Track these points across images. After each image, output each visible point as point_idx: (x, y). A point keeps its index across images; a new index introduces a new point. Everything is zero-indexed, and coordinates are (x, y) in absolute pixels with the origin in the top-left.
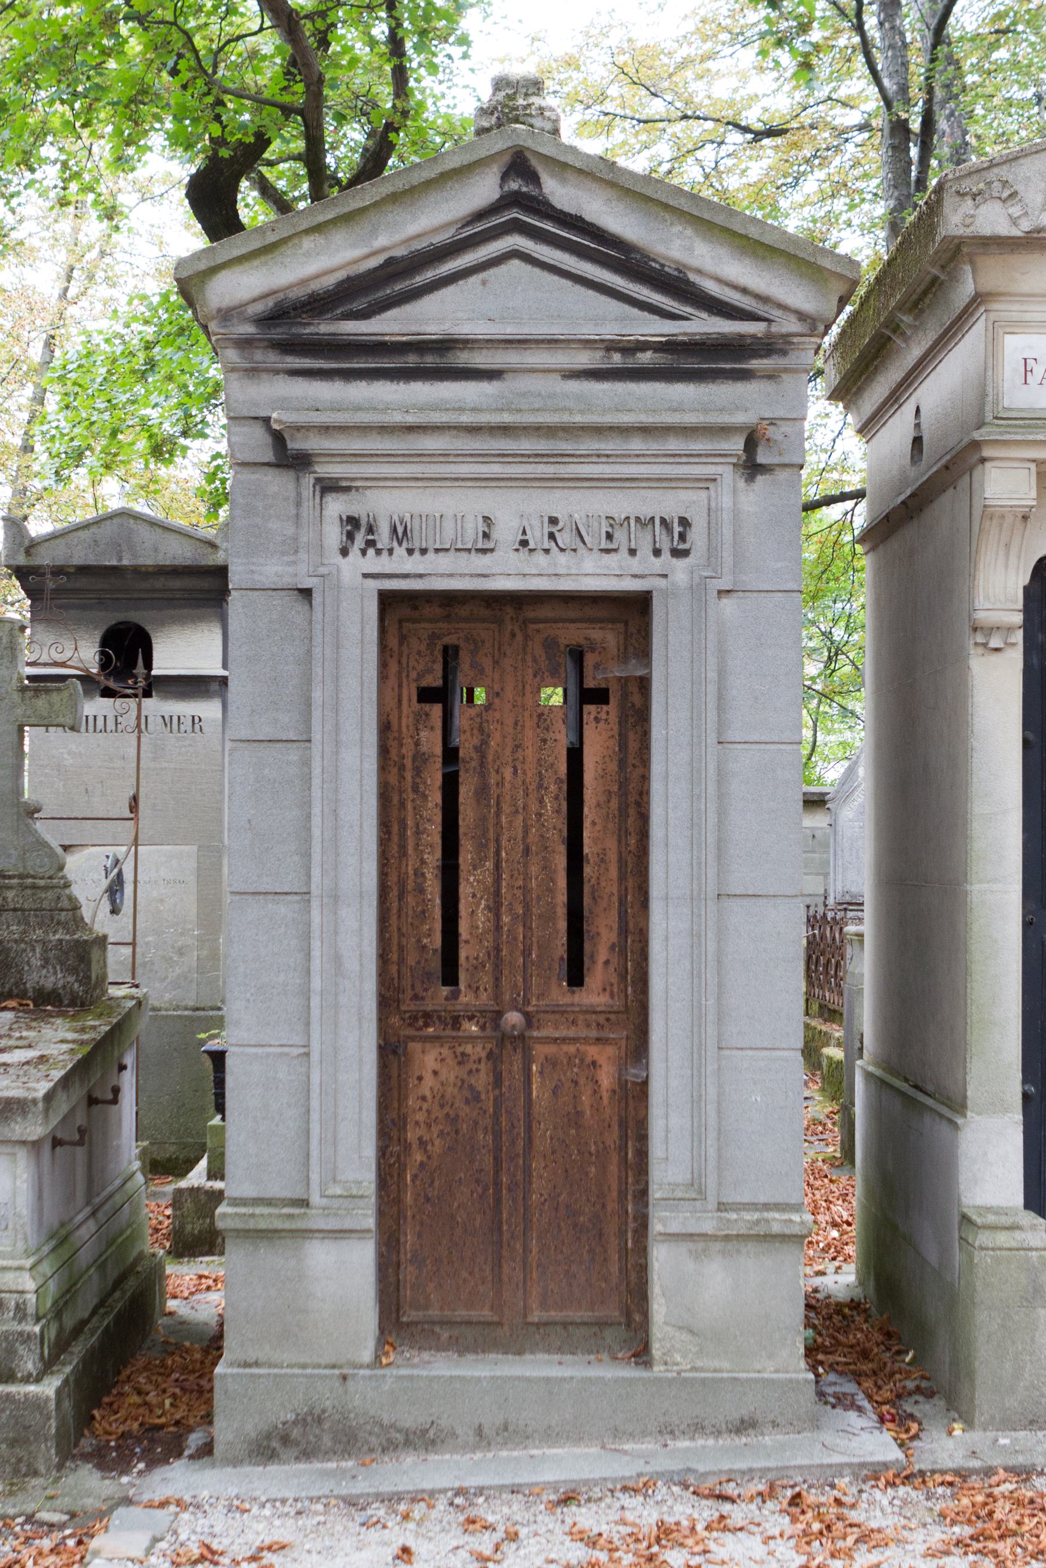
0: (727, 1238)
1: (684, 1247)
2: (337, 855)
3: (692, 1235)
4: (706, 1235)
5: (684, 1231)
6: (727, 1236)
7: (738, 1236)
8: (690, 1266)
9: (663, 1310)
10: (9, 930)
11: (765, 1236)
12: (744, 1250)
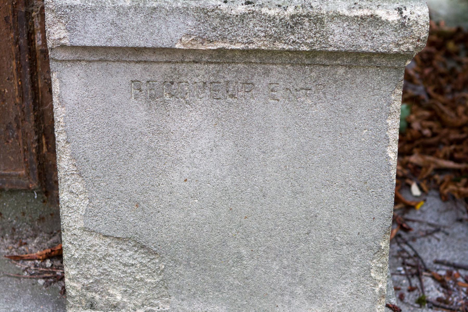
0: (222, 56)
1: (122, 76)
2: (114, 62)
3: (137, 50)
4: (171, 51)
5: (116, 42)
6: (221, 52)
7: (246, 52)
8: (137, 114)
9: (82, 204)
10: (465, 216)
11: (313, 54)
12: (262, 83)
